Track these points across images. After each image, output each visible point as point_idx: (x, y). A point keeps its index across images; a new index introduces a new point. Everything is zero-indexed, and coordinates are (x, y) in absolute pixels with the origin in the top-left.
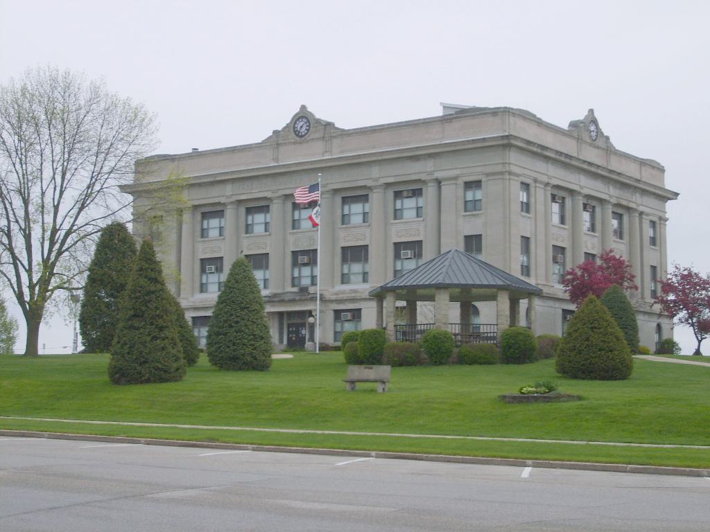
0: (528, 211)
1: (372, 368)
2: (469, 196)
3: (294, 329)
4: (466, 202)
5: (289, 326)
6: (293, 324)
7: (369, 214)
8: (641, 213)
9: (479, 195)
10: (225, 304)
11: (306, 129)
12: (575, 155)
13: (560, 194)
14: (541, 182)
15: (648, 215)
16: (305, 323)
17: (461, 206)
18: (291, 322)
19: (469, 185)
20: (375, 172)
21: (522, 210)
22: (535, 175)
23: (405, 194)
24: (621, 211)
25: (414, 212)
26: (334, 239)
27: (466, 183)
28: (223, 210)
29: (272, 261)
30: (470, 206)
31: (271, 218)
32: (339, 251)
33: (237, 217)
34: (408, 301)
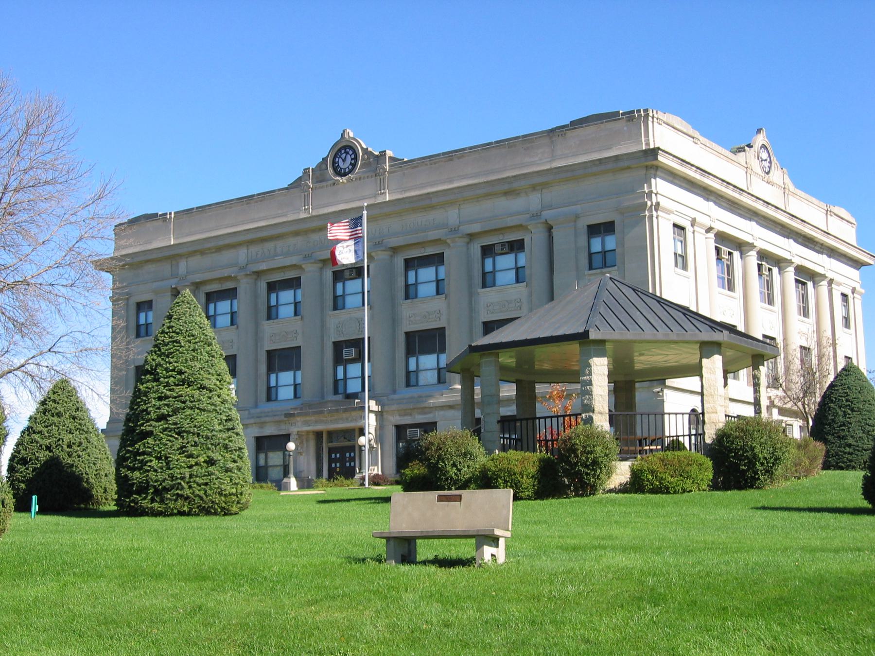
0: (685, 267)
1: (459, 498)
2: (596, 245)
3: (338, 456)
4: (590, 255)
5: (331, 451)
6: (336, 448)
7: (446, 282)
8: (831, 282)
9: (611, 242)
10: (164, 349)
11: (351, 164)
12: (745, 188)
13: (726, 242)
14: (701, 226)
15: (839, 284)
16: (354, 447)
17: (584, 261)
18: (334, 444)
19: (594, 230)
20: (452, 216)
21: (676, 265)
22: (694, 214)
23: (498, 249)
24: (806, 276)
25: (512, 274)
26: (394, 321)
27: (590, 227)
28: (236, 288)
29: (308, 359)
30: (598, 260)
31: (303, 296)
32: (402, 339)
33: (255, 296)
34: (518, 383)
